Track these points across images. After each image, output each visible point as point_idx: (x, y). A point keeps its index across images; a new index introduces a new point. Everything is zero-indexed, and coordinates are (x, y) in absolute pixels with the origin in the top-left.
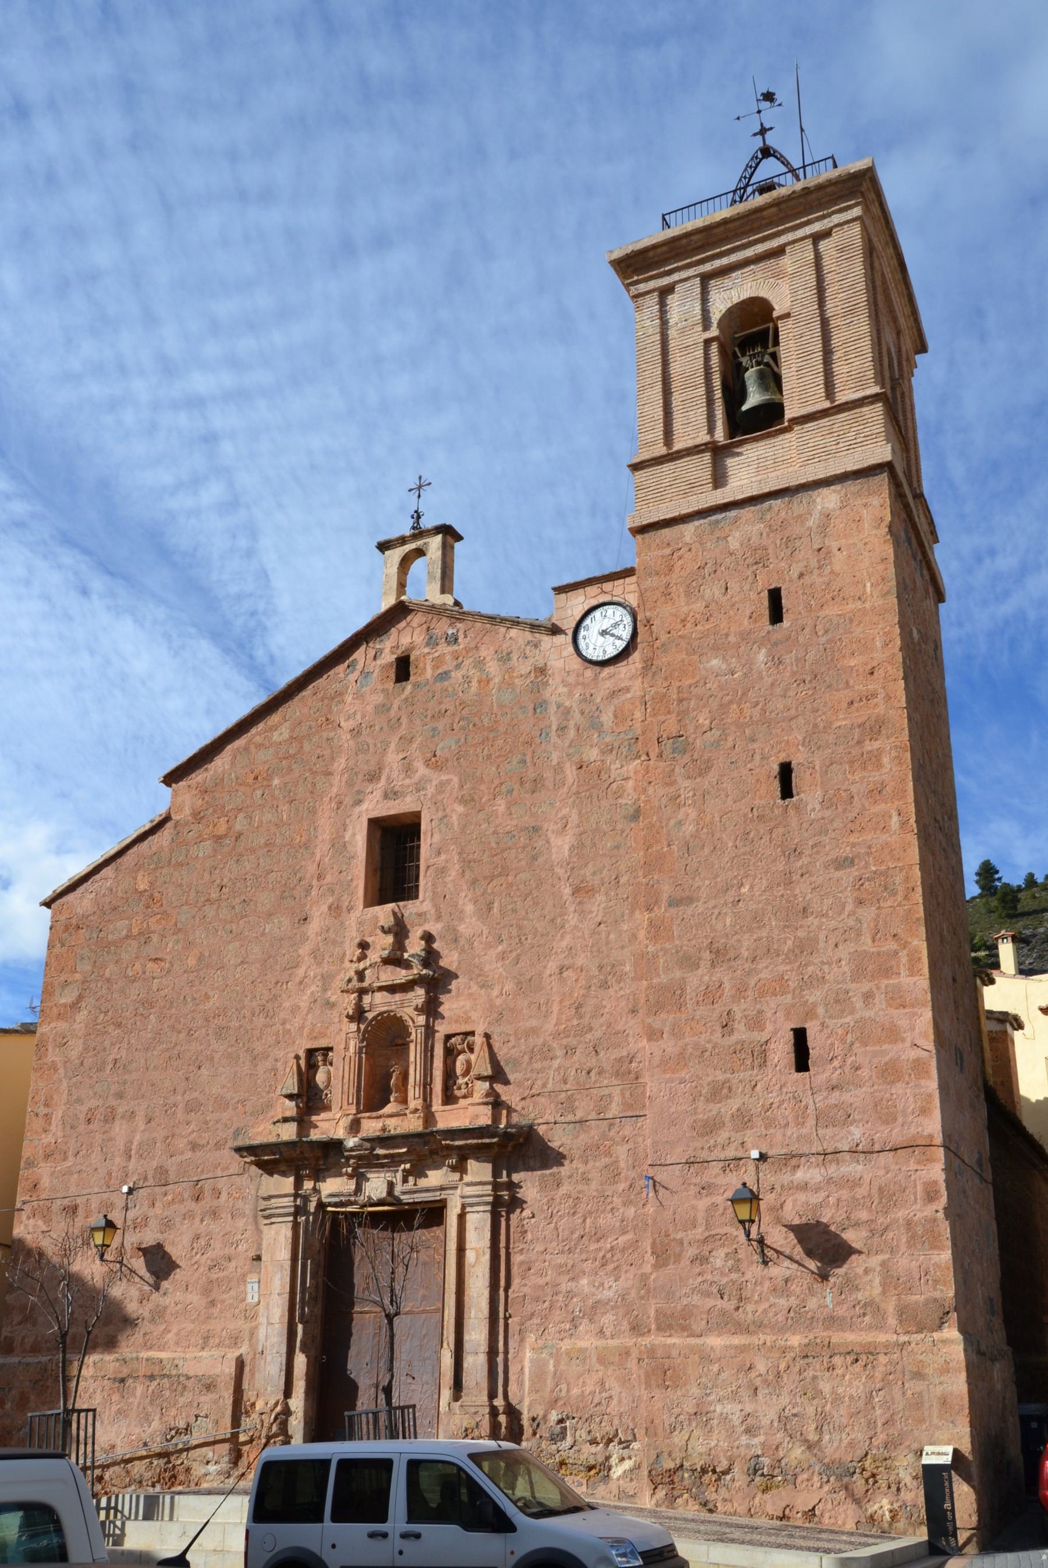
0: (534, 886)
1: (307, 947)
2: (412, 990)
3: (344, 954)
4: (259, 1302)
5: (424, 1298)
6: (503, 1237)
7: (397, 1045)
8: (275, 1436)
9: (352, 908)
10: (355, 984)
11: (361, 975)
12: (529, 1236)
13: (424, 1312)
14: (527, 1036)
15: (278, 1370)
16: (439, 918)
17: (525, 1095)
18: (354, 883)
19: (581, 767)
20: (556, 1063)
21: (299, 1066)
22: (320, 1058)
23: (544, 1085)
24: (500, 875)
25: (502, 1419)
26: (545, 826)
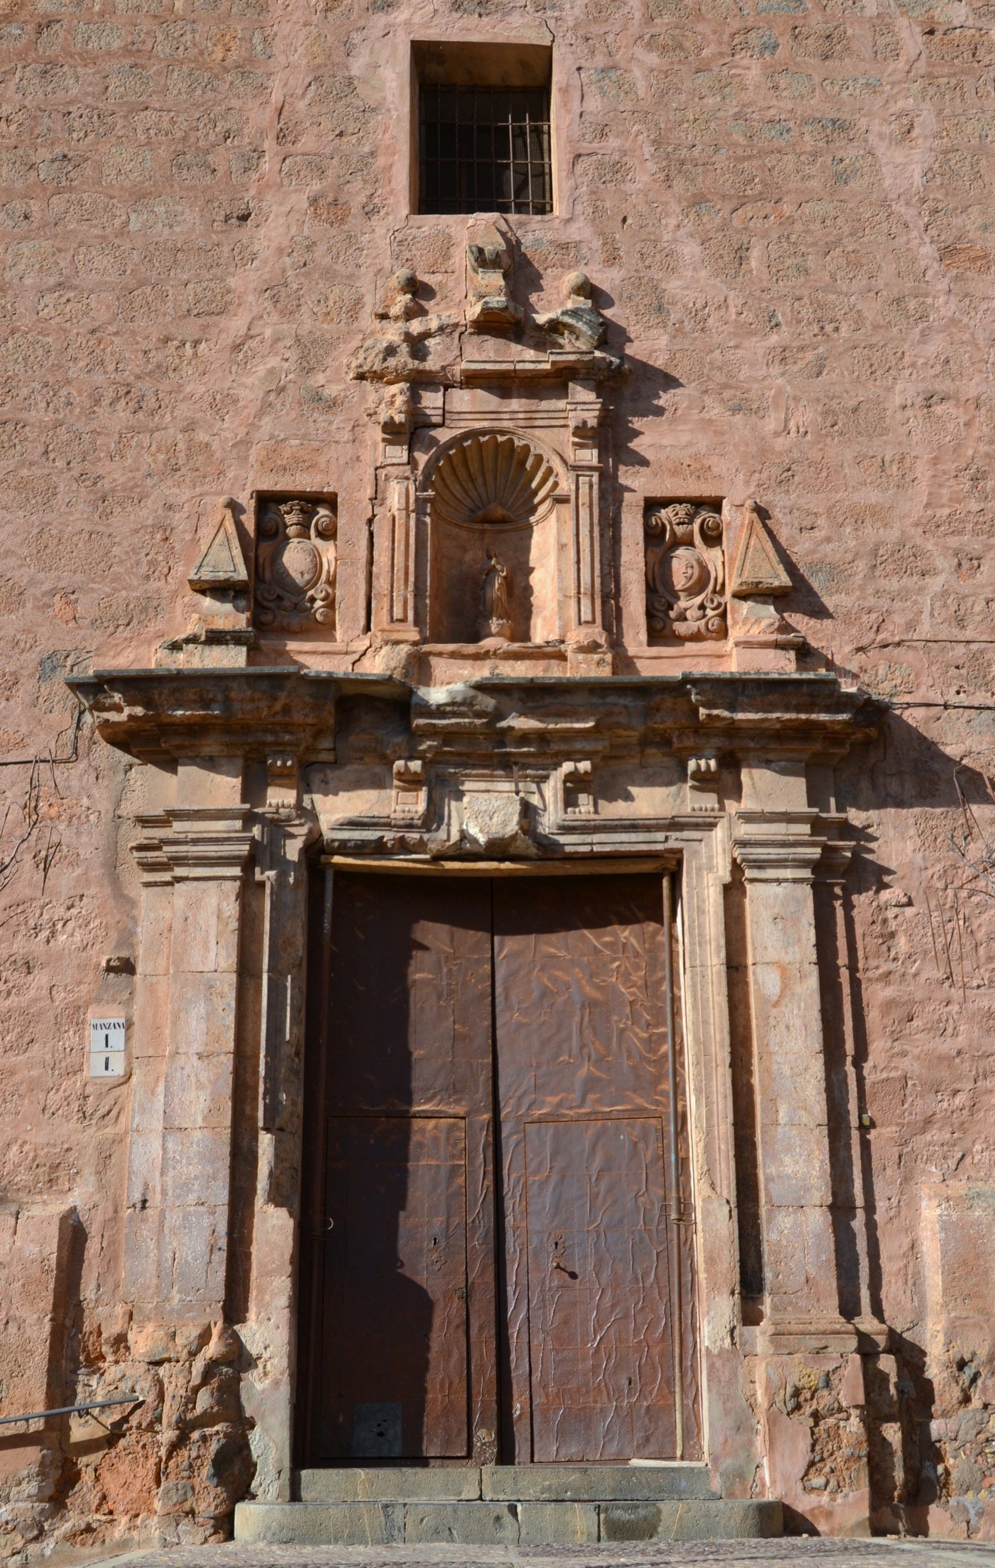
0: (846, 230)
1: (252, 276)
2: (562, 391)
3: (359, 302)
4: (129, 1076)
5: (591, 1084)
6: (842, 943)
7: (485, 520)
8: (207, 1419)
9: (376, 210)
10: (403, 359)
11: (417, 345)
12: (902, 944)
13: (593, 1116)
14: (859, 522)
15: (202, 1248)
16: (612, 259)
17: (865, 642)
18: (381, 161)
19: (931, 32)
20: (935, 584)
21: (239, 526)
22: (290, 519)
23: (911, 626)
24: (760, 197)
25: (887, 1364)
26: (863, 123)
